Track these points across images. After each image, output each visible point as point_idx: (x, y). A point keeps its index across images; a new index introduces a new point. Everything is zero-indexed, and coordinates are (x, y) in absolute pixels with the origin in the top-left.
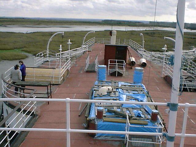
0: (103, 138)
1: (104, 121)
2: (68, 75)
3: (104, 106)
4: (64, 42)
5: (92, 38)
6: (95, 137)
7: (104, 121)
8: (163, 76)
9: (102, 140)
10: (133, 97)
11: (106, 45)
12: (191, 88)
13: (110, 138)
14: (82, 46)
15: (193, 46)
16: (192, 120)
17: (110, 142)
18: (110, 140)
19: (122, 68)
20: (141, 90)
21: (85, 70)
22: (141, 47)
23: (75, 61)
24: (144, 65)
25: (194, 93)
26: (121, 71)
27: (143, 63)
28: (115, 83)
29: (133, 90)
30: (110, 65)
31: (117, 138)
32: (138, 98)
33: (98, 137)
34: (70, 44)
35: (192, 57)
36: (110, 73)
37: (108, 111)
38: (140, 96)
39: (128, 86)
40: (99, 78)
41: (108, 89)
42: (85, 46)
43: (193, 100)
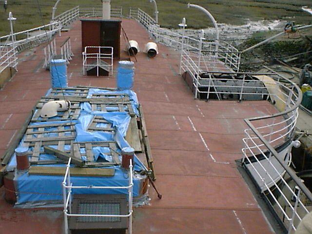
0: (31, 205)
1: (30, 174)
2: (12, 78)
3: (40, 141)
4: (34, 15)
5: (73, 7)
6: (16, 204)
7: (30, 174)
8: (181, 73)
9: (29, 210)
10: (105, 118)
11: (83, 22)
12: (223, 94)
13: (45, 205)
14: (51, 22)
15: (247, 18)
16: (211, 156)
17: (43, 212)
18: (44, 208)
19: (109, 61)
20: (126, 102)
21: (44, 67)
22: (153, 22)
23: (35, 49)
24: (152, 53)
25: (227, 102)
26: (105, 67)
27: (134, 48)
28: (82, 90)
29: (110, 104)
30: (111, 56)
31: (57, 203)
32: (113, 121)
33: (21, 204)
34: (13, 20)
35: (243, 37)
36: (88, 70)
37: (45, 151)
38: (117, 116)
39: (104, 97)
40: (53, 84)
41: (59, 106)
42: (56, 22)
43: (223, 115)
